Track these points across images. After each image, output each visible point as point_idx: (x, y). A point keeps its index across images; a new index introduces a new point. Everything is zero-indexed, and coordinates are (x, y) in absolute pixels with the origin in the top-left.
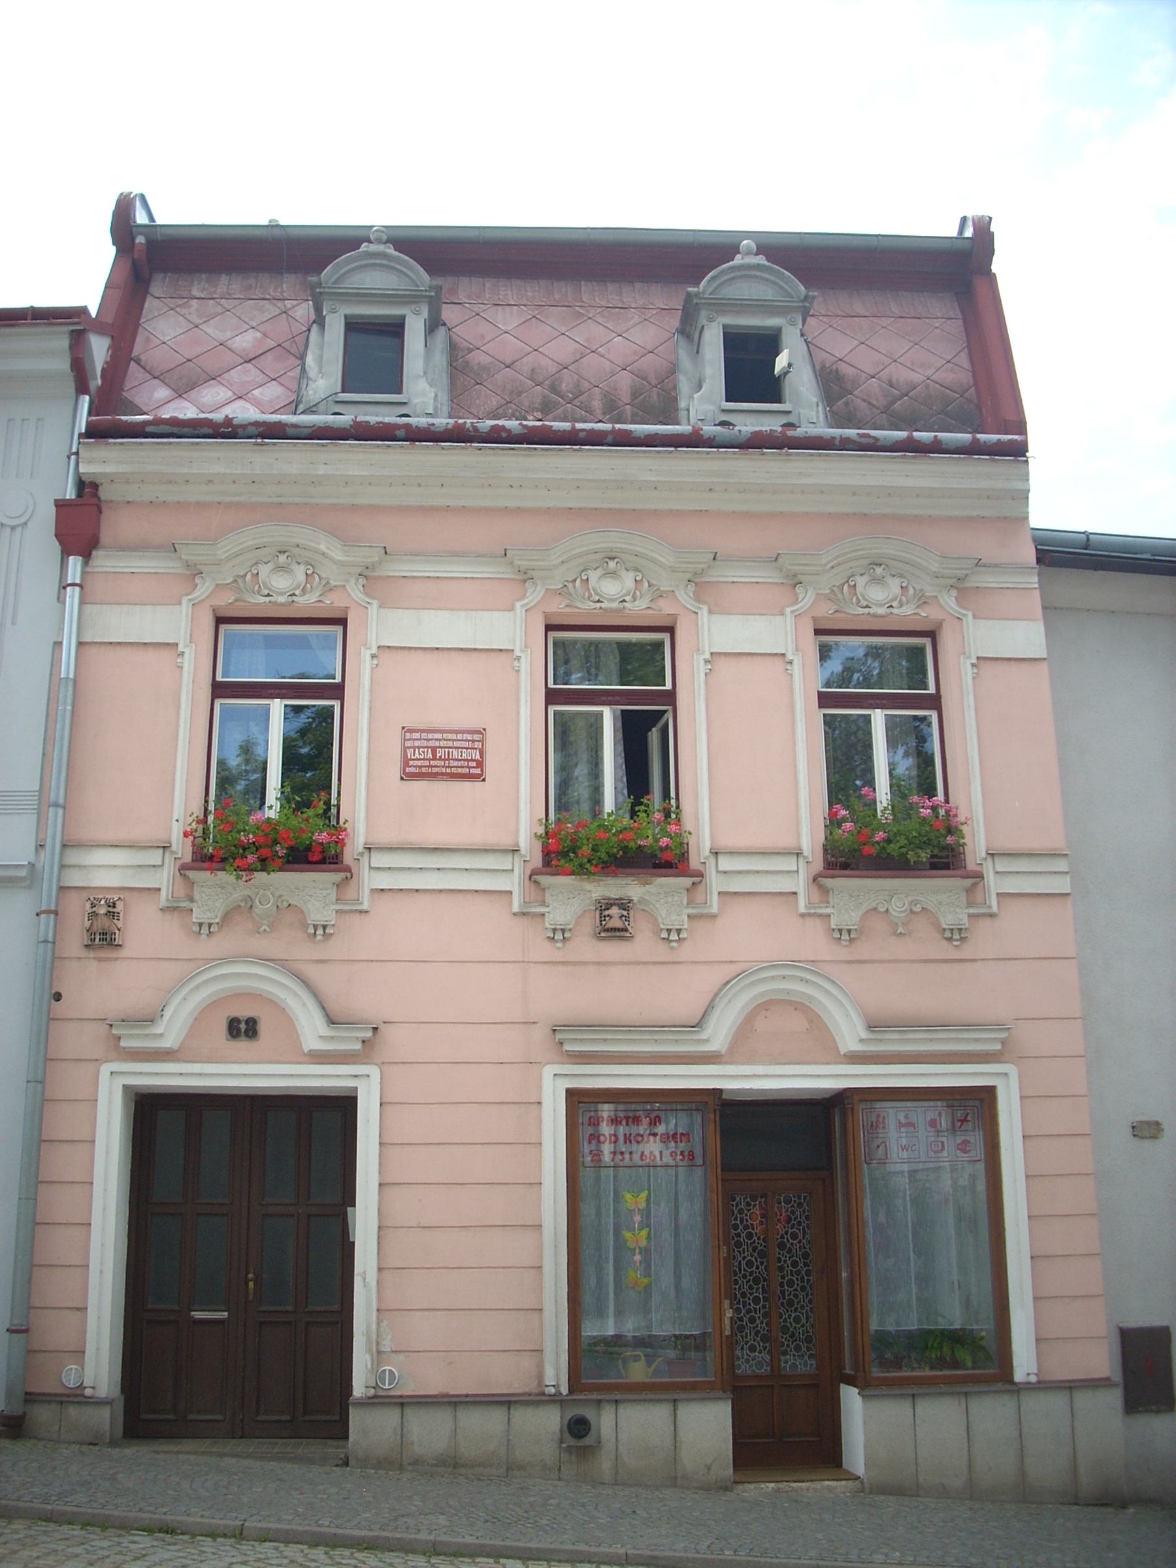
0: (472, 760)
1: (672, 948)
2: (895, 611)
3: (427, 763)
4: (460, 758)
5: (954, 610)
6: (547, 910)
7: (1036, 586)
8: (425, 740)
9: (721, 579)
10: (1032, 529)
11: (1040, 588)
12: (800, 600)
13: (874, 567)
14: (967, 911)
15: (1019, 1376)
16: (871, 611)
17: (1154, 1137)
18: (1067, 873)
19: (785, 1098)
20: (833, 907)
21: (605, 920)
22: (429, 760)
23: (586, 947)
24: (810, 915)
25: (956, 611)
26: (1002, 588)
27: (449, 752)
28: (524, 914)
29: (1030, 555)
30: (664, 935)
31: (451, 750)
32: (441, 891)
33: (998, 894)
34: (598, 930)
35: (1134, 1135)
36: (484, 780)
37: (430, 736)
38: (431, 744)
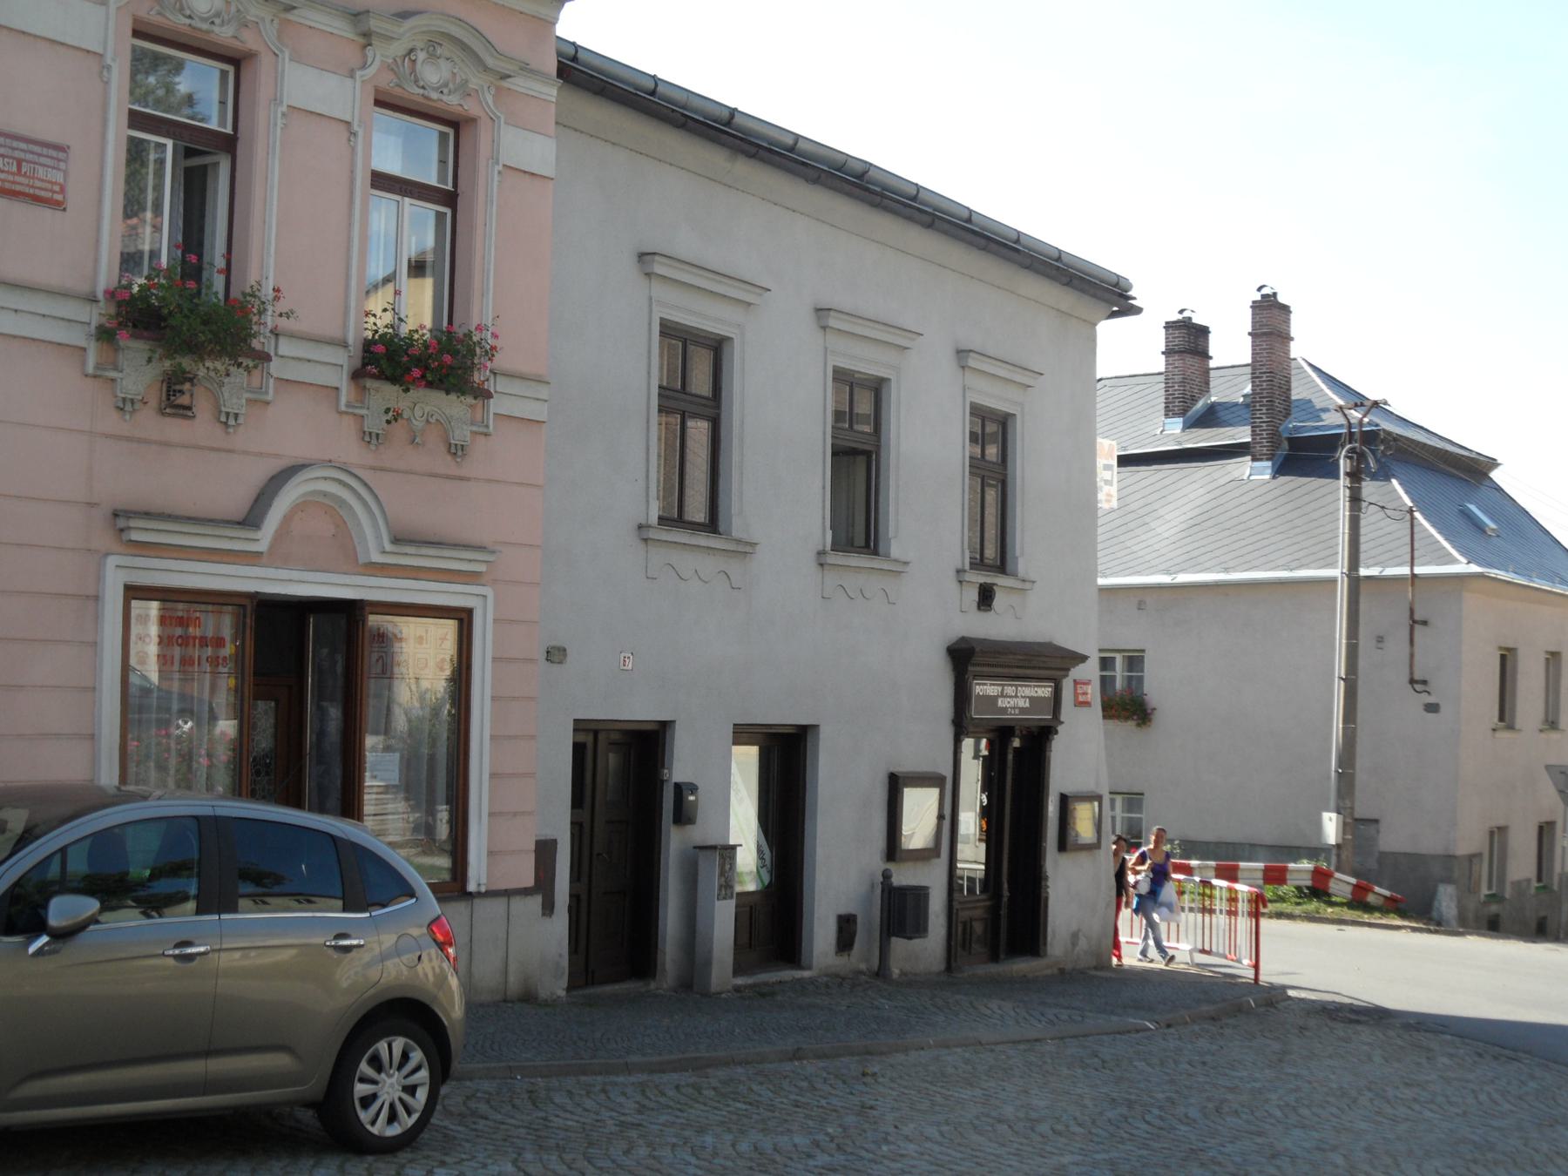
0: (56, 183)
1: (228, 433)
2: (445, 98)
3: (11, 178)
4: (45, 178)
5: (489, 107)
6: (120, 375)
7: (554, 100)
8: (9, 147)
9: (302, 21)
10: (558, 37)
11: (557, 103)
12: (369, 63)
13: (435, 44)
14: (470, 428)
15: (472, 887)
16: (426, 93)
17: (560, 662)
18: (546, 401)
19: (1049, 774)
20: (368, 408)
21: (174, 395)
22: (13, 174)
23: (150, 423)
24: (346, 413)
25: (492, 111)
26: (528, 95)
27: (34, 169)
28: (95, 376)
29: (552, 68)
30: (223, 419)
31: (36, 166)
32: (15, 337)
33: (494, 414)
34: (163, 406)
35: (547, 660)
36: (64, 210)
37: (15, 144)
38: (17, 154)
